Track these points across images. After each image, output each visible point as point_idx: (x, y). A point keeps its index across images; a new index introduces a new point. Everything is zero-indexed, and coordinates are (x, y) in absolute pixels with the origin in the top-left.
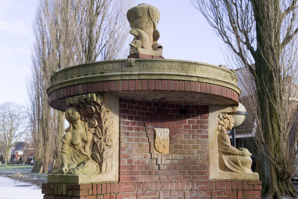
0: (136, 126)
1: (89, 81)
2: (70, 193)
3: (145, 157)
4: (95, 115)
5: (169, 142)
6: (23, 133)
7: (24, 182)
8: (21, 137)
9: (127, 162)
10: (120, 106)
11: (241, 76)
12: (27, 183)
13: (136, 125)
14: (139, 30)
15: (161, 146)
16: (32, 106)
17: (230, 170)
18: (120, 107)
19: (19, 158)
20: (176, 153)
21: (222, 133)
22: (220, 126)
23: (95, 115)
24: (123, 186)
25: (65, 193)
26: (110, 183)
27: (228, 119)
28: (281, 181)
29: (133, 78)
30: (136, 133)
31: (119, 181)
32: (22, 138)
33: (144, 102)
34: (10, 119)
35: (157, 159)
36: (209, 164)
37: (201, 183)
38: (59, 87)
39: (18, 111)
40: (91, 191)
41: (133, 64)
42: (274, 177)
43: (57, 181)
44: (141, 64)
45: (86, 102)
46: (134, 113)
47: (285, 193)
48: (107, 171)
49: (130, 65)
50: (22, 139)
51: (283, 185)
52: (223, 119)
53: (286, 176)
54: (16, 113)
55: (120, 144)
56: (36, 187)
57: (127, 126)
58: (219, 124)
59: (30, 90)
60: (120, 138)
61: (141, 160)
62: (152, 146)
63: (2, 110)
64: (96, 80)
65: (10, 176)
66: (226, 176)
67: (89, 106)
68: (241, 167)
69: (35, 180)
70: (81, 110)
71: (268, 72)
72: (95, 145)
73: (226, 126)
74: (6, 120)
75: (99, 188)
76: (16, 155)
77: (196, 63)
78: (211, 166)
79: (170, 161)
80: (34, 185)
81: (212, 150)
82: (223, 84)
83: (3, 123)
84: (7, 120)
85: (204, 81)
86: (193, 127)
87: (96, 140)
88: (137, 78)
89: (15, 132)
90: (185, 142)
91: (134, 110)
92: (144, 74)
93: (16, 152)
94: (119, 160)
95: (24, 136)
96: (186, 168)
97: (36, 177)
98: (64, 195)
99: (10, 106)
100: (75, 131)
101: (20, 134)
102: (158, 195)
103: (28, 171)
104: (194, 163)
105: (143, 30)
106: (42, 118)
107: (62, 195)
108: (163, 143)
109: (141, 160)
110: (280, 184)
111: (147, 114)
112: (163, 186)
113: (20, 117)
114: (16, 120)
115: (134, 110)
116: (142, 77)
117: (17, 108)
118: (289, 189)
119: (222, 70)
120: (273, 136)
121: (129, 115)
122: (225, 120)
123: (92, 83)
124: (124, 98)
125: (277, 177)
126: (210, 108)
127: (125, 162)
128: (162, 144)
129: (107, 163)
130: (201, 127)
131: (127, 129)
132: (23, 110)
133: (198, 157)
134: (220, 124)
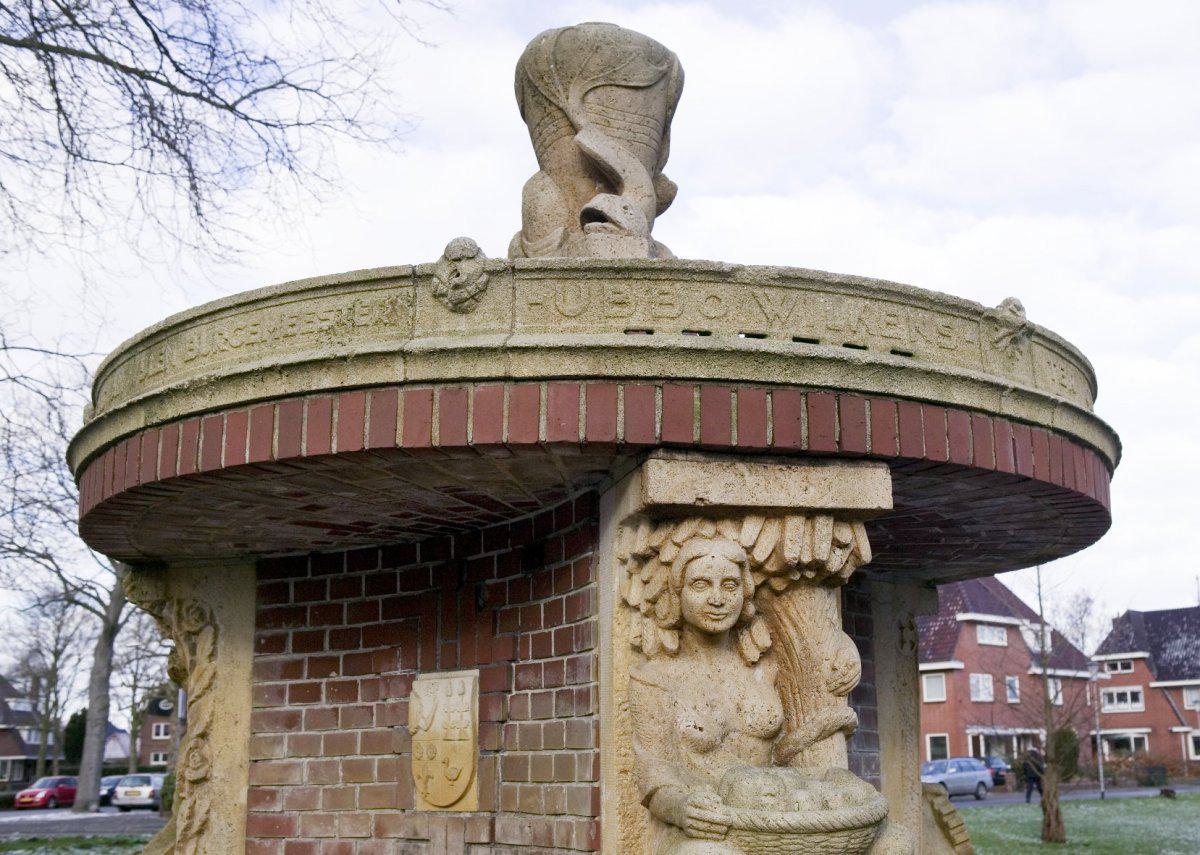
0: (335, 677)
10: (263, 593)
13: (333, 674)
30: (336, 710)
33: (380, 553)
46: (331, 614)
57: (288, 682)
77: (418, 273)
91: (328, 599)
115: (328, 599)
119: (310, 295)
121: (303, 629)
124: (268, 556)
125: (37, 821)
131: (287, 697)
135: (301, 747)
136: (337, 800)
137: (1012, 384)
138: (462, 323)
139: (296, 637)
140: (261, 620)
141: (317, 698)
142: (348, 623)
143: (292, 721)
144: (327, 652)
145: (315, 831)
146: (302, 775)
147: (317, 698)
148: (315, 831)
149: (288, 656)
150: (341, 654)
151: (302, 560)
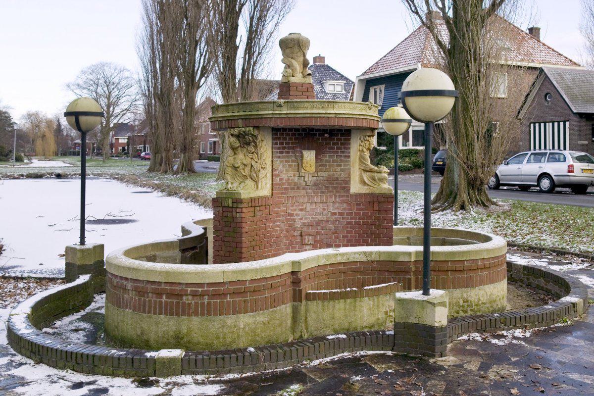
0: (286, 150)
1: (247, 117)
2: (235, 205)
3: (294, 176)
4: (253, 143)
5: (315, 162)
6: (127, 110)
7: (140, 186)
8: (124, 116)
9: (278, 180)
11: (446, 38)
12: (145, 188)
14: (290, 59)
15: (308, 165)
16: (145, 74)
17: (368, 185)
18: (273, 135)
19: (120, 148)
20: (321, 170)
21: (362, 154)
22: (361, 147)
23: (253, 143)
24: (275, 200)
25: (231, 205)
26: (265, 197)
27: (368, 141)
28: (473, 187)
29: (283, 116)
31: (272, 195)
32: (125, 117)
34: (105, 89)
35: (304, 177)
36: (350, 181)
37: (343, 196)
38: (221, 119)
39: (119, 75)
40: (250, 203)
41: (282, 105)
42: (463, 183)
43: (224, 196)
44: (289, 104)
45: (245, 134)
46: (285, 139)
47: (476, 202)
48: (263, 188)
49: (280, 106)
50: (127, 119)
51: (475, 193)
52: (363, 141)
53: (478, 182)
54: (115, 79)
55: (272, 166)
56: (160, 194)
58: (360, 145)
59: (142, 49)
60: (272, 161)
61: (291, 178)
62: (300, 165)
63: (94, 74)
64: (253, 117)
65: (116, 178)
66: (365, 190)
67: (247, 137)
68: (378, 184)
69: (156, 184)
70: (240, 139)
71: (463, 53)
72: (253, 168)
73: (367, 147)
74: (100, 90)
75: (257, 202)
76: (115, 144)
78: (352, 182)
79: (316, 178)
80: (156, 191)
81: (353, 168)
82: (358, 117)
83: (95, 95)
84: (102, 91)
85: (341, 116)
86: (337, 148)
87: (253, 163)
88: (285, 116)
89: (114, 109)
90: (330, 161)
92: (291, 114)
93: (116, 139)
94: (272, 178)
95: (129, 115)
96: (330, 183)
97: (157, 180)
98: (230, 207)
99: (105, 68)
100: (236, 156)
101: (122, 111)
102: (305, 206)
103: (142, 170)
104: (337, 179)
105: (294, 59)
106: (161, 92)
107: (228, 207)
108: (309, 162)
109: (291, 178)
110: (471, 191)
111: (296, 139)
112: (309, 199)
113: (121, 85)
114: (115, 90)
116: (290, 116)
117: (117, 71)
118: (482, 198)
120: (466, 134)
122: (365, 142)
123: (250, 119)
126: (352, 131)
127: (277, 180)
128: (309, 164)
129: (262, 182)
130: (344, 148)
132: (126, 74)
133: (341, 174)
134: (362, 146)
135: (281, 162)
136: (287, 170)
137: (120, 275)
138: (369, 111)
139: (286, 142)
140: (273, 139)
141: (342, 141)
142: (413, 146)
143: (279, 157)
144: (284, 146)
145: (284, 176)
146: (281, 167)
147: (289, 153)
148: (284, 176)
149: (278, 146)
150: (287, 146)
151: (280, 129)
